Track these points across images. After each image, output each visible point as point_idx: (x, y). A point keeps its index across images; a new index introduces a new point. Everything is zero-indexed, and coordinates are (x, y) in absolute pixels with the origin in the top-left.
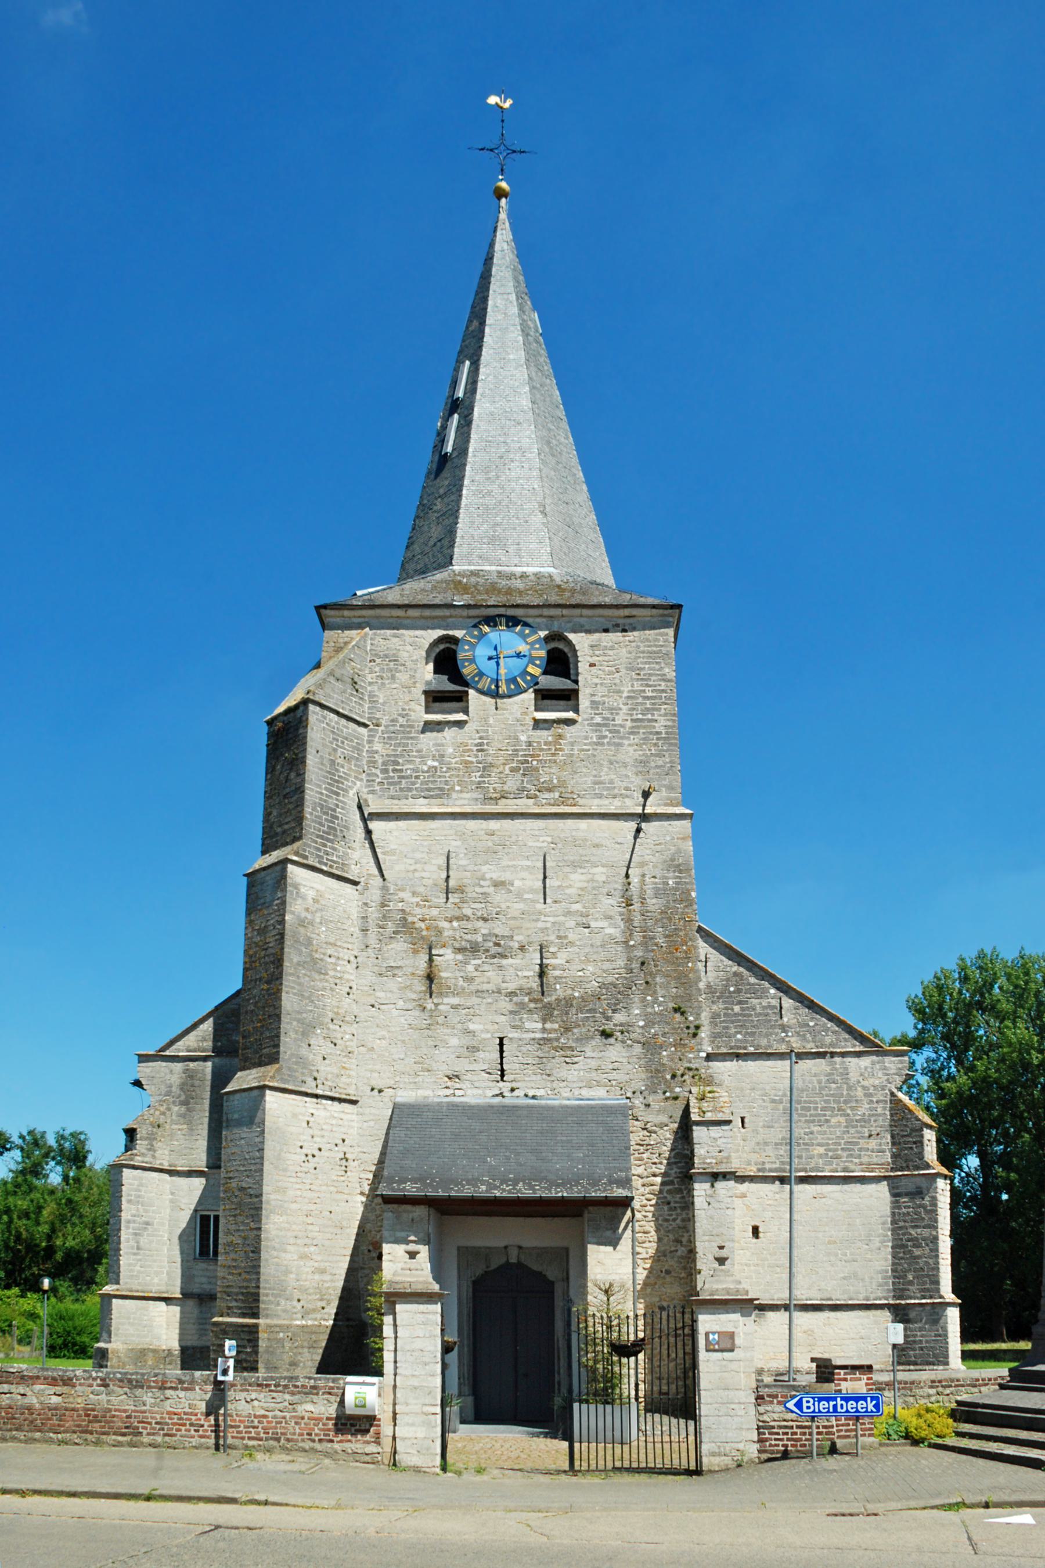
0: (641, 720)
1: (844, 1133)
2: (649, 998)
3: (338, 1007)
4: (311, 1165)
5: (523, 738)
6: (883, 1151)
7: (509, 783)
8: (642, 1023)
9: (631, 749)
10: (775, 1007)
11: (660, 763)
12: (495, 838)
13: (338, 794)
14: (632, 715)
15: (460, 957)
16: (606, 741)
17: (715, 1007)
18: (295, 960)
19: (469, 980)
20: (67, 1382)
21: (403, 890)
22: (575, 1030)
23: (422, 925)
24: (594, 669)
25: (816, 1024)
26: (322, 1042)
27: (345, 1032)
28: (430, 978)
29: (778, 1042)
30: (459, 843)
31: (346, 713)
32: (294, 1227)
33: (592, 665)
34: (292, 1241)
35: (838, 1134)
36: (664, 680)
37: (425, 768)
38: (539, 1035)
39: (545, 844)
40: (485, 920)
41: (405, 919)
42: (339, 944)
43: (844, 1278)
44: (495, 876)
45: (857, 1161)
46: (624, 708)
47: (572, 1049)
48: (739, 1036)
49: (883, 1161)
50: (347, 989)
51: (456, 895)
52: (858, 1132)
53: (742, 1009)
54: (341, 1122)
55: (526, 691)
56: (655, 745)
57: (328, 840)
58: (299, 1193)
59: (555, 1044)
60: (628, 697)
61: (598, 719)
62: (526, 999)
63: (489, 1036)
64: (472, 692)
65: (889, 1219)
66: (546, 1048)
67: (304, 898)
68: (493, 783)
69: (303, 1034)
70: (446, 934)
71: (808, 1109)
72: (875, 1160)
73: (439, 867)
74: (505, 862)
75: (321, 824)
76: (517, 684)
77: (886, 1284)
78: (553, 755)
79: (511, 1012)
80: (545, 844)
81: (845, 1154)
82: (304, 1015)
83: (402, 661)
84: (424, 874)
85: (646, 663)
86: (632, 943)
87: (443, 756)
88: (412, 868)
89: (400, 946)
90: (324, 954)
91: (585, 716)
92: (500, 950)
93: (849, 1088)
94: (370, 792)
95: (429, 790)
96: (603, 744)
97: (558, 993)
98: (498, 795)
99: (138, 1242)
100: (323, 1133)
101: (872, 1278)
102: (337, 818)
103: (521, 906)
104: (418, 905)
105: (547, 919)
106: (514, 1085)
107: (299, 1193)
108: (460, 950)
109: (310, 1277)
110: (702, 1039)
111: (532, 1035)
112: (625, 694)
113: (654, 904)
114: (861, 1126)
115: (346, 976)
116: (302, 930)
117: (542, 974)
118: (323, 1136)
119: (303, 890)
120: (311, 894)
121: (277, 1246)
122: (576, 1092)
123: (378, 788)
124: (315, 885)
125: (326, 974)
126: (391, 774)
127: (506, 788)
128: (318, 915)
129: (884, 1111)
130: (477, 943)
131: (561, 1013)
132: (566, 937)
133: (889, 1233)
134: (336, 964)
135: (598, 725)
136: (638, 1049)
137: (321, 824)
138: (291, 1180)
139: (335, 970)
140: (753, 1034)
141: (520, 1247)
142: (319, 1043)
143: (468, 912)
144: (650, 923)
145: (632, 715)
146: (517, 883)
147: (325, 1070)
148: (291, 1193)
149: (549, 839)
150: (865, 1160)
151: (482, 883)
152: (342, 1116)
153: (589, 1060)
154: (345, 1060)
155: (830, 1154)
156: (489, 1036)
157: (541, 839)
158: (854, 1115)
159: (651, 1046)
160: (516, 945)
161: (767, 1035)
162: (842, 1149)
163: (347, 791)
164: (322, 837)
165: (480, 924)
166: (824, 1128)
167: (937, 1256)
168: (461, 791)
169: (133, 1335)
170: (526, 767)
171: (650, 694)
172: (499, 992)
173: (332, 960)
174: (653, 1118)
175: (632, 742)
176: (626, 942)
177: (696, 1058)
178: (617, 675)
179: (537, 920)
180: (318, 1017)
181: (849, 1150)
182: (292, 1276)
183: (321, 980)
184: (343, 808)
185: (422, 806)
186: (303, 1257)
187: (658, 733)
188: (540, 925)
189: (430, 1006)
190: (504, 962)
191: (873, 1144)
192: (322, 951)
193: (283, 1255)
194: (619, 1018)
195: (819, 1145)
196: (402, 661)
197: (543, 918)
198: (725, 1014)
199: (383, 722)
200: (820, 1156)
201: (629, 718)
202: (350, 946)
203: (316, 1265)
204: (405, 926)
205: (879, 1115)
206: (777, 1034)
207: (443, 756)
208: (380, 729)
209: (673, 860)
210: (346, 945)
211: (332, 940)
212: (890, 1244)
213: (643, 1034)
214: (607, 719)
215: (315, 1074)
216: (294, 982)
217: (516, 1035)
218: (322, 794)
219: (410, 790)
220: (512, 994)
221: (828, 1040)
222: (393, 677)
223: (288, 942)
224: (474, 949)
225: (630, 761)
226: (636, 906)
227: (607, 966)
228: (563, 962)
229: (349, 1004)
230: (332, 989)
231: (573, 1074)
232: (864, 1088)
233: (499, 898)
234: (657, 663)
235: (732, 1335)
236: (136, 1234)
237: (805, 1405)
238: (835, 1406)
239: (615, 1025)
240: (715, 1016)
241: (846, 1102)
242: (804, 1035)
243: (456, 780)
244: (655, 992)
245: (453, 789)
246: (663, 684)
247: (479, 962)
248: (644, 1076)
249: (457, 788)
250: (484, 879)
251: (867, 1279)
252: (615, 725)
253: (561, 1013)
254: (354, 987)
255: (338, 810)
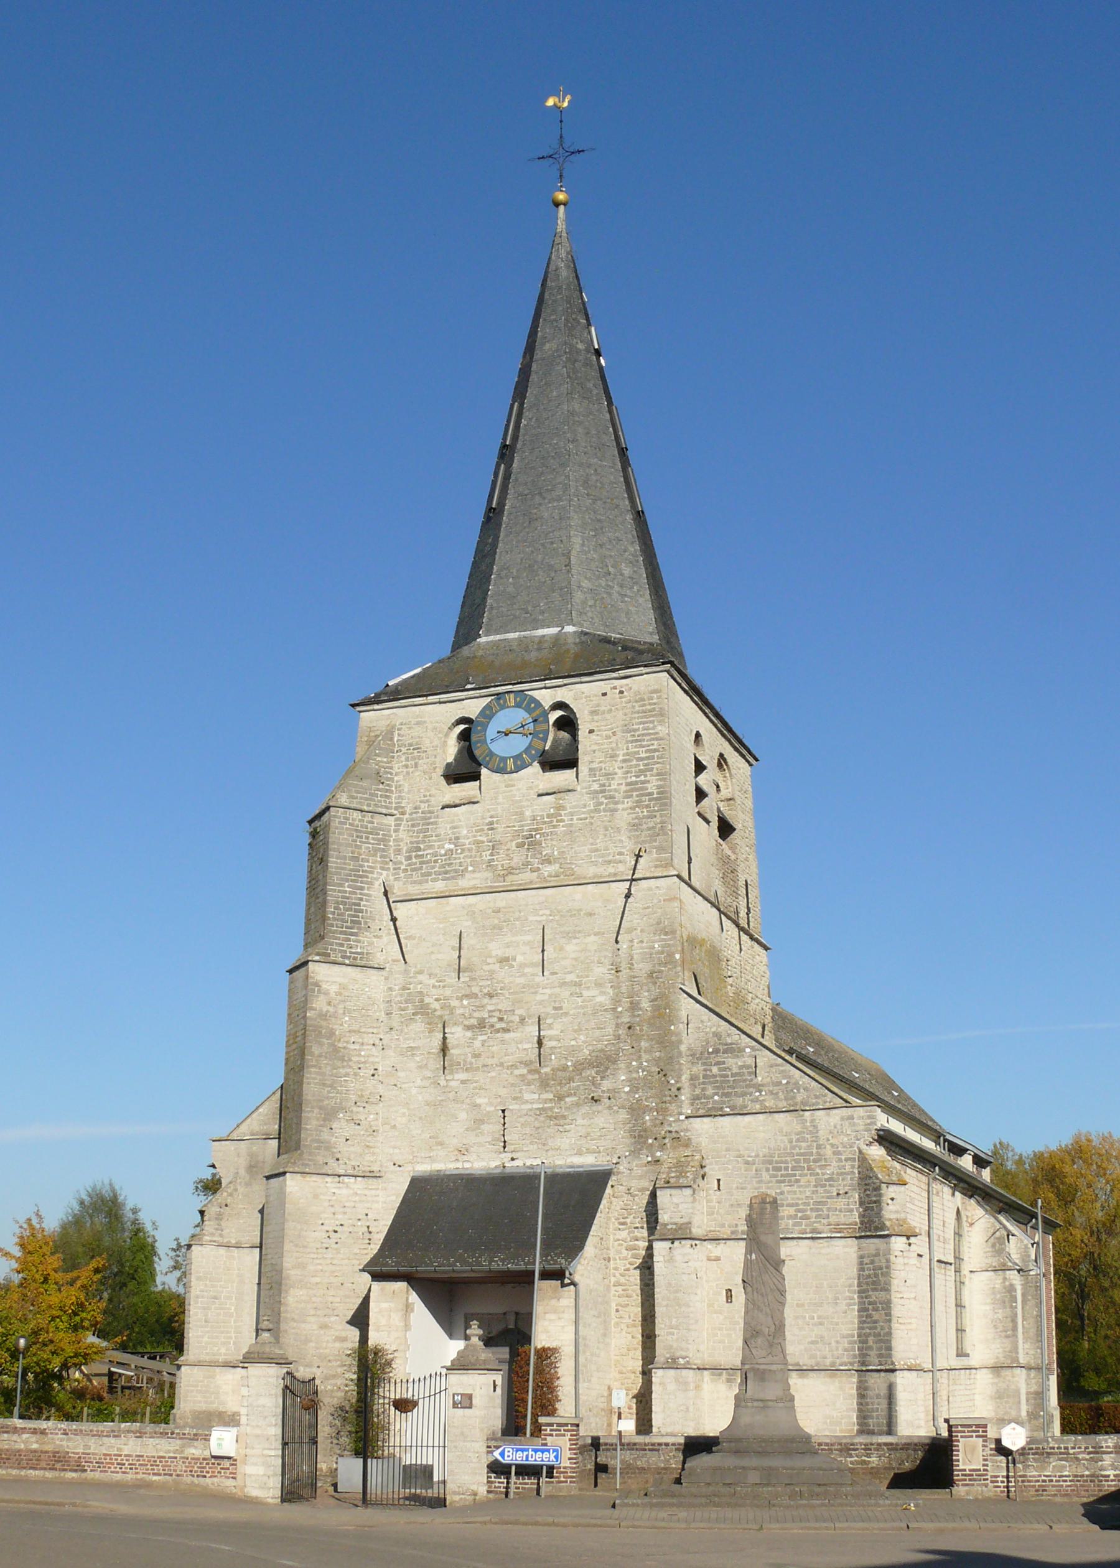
0: (636, 783)
1: (813, 1192)
2: (634, 1063)
3: (362, 1090)
4: (333, 1241)
5: (528, 813)
6: (851, 1211)
7: (515, 860)
8: (627, 1089)
9: (625, 813)
10: (748, 1067)
11: (651, 825)
12: (500, 915)
13: (362, 888)
14: (626, 778)
15: (469, 1034)
16: (602, 807)
17: (695, 1069)
18: (317, 1053)
19: (476, 1056)
20: (43, 1432)
21: (421, 972)
22: (567, 1099)
23: (436, 1005)
24: (593, 736)
25: (788, 1083)
26: (343, 1124)
27: (369, 1113)
28: (444, 1049)
29: (752, 1101)
30: (469, 923)
31: (371, 809)
32: (314, 1299)
33: (591, 731)
34: (312, 1312)
35: (808, 1194)
36: (657, 739)
37: (443, 852)
38: (535, 1106)
39: (544, 918)
40: (491, 996)
41: (422, 1001)
42: (363, 1030)
43: (812, 1342)
44: (500, 953)
45: (825, 1221)
46: (619, 772)
47: (564, 1117)
48: (716, 1098)
49: (851, 1221)
50: (372, 1072)
51: (466, 974)
52: (826, 1192)
53: (720, 1069)
54: (364, 1198)
55: (530, 764)
56: (647, 806)
57: (352, 934)
58: (320, 1267)
59: (550, 1113)
60: (624, 761)
61: (596, 787)
62: (525, 1071)
63: (492, 1109)
64: (484, 772)
65: (856, 1282)
66: (542, 1118)
67: (326, 993)
68: (501, 861)
69: (324, 1120)
70: (459, 1011)
71: (779, 1169)
72: (843, 1220)
73: (453, 948)
74: (509, 938)
75: (343, 921)
76: (523, 760)
77: (853, 1349)
78: (554, 827)
79: (512, 1085)
80: (544, 918)
81: (814, 1214)
82: (326, 1102)
83: (424, 749)
84: (440, 956)
85: (641, 723)
86: (620, 1009)
87: (457, 838)
88: (431, 949)
89: (419, 1026)
90: (347, 1042)
91: (584, 785)
92: (503, 1025)
93: (819, 1147)
94: (396, 879)
95: (446, 873)
96: (599, 811)
97: (553, 1062)
98: (505, 872)
99: (206, 1315)
100: (345, 1210)
101: (837, 1342)
102: (361, 911)
103: (521, 980)
104: (434, 986)
105: (545, 991)
106: (514, 1155)
107: (320, 1267)
108: (469, 1028)
109: (330, 1345)
110: (682, 1102)
111: (530, 1106)
112: (621, 758)
113: (642, 968)
114: (830, 1186)
115: (371, 1059)
116: (323, 1023)
117: (540, 1043)
118: (345, 1213)
119: (324, 986)
120: (333, 989)
121: (296, 1317)
122: (569, 1161)
123: (402, 875)
124: (338, 979)
125: (350, 1060)
126: (414, 860)
127: (512, 864)
128: (341, 1006)
129: (852, 1169)
130: (484, 1019)
131: (568, 1080)
132: (561, 1008)
133: (856, 1296)
134: (360, 1050)
135: (596, 792)
136: (623, 1115)
137: (343, 921)
138: (312, 1256)
139: (360, 1055)
140: (727, 1095)
141: (517, 1314)
142: (342, 1126)
143: (475, 990)
144: (637, 988)
145: (626, 778)
146: (520, 958)
147: (344, 1149)
148: (311, 1268)
149: (548, 912)
150: (833, 1219)
151: (489, 960)
152: (366, 1192)
153: (580, 1128)
154: (369, 1139)
155: (800, 1215)
156: (492, 1109)
157: (541, 913)
158: (823, 1174)
159: (636, 1110)
160: (517, 1019)
161: (744, 1094)
162: (812, 1209)
163: (371, 883)
164: (345, 933)
165: (486, 1001)
166: (795, 1188)
167: (890, 1321)
168: (474, 871)
169: (200, 1402)
170: (530, 842)
171: (644, 755)
172: (502, 1064)
173: (357, 1047)
174: (635, 1184)
175: (626, 806)
176: (614, 1009)
177: (674, 1123)
178: (613, 739)
179: (536, 993)
180: (341, 1103)
181: (818, 1210)
182: (312, 1344)
183: (343, 1067)
184: (367, 901)
185: (440, 886)
186: (324, 1326)
187: (651, 794)
188: (539, 997)
189: (443, 1083)
190: (507, 1036)
191: (841, 1203)
192: (346, 1039)
193: (303, 1325)
194: (606, 1085)
195: (788, 1205)
196: (424, 749)
197: (541, 991)
198: (705, 1076)
199: (408, 811)
200: (790, 1217)
201: (623, 782)
202: (375, 1031)
203: (337, 1334)
204: (423, 1010)
205: (847, 1174)
206: (751, 1094)
207: (457, 838)
208: (405, 817)
209: (658, 923)
210: (371, 1030)
211: (355, 1027)
212: (856, 1307)
213: (628, 1100)
214: (604, 785)
215: (338, 1156)
216: (316, 1073)
217: (516, 1107)
218: (345, 892)
219: (429, 874)
220: (513, 1067)
221: (799, 1098)
222: (416, 765)
223: (311, 1036)
224: (481, 1025)
225: (623, 825)
226: (625, 973)
227: (597, 1033)
228: (558, 1032)
229: (374, 1086)
230: (356, 1074)
231: (564, 1142)
232: (832, 1145)
233: (503, 974)
234: (651, 722)
235: (470, 1397)
236: (204, 1308)
237: (506, 1454)
238: (527, 1456)
239: (603, 1092)
240: (693, 1078)
241: (815, 1161)
242: (777, 1094)
243: (469, 860)
244: (640, 1057)
245: (466, 868)
246: (656, 742)
247: (484, 1037)
248: (628, 1141)
249: (470, 868)
250: (491, 957)
251: (834, 1344)
252: (610, 791)
253: (568, 1080)
254: (380, 1069)
255: (362, 903)
